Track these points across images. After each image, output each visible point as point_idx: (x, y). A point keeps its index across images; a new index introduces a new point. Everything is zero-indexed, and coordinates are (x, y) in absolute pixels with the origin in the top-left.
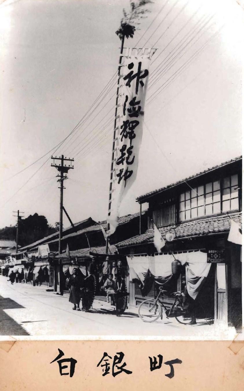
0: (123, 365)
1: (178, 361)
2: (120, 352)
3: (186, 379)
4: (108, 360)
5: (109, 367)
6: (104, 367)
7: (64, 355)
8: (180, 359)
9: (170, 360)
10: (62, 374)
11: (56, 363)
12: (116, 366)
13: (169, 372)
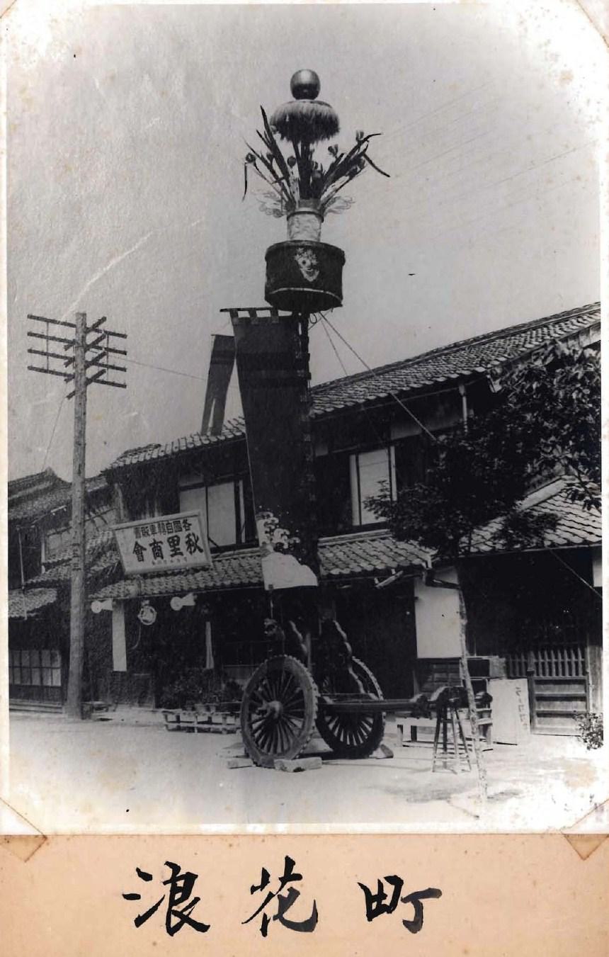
1: (433, 893)
10: (584, 858)
13: (411, 917)
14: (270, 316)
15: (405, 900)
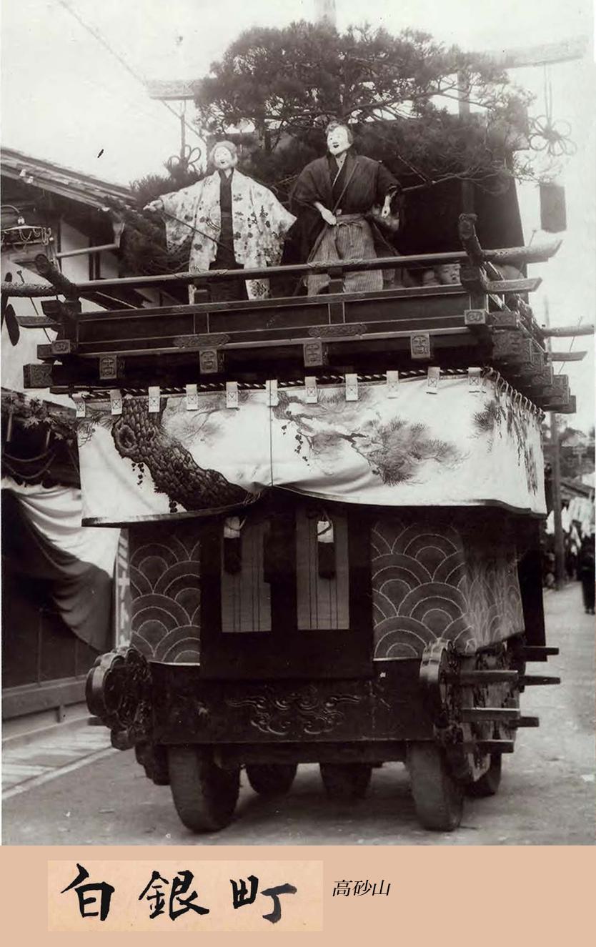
0: (191, 897)
1: (288, 889)
2: (184, 870)
3: (305, 924)
4: (160, 887)
5: (163, 901)
6: (154, 901)
7: (88, 876)
8: (292, 884)
9: (273, 887)
10: (84, 915)
11: (73, 893)
12: (178, 899)
13: (270, 910)
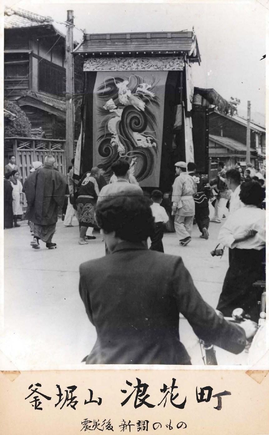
1: (226, 393)
13: (216, 405)
14: (208, 390)
15: (214, 396)
